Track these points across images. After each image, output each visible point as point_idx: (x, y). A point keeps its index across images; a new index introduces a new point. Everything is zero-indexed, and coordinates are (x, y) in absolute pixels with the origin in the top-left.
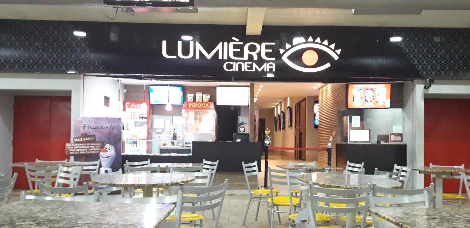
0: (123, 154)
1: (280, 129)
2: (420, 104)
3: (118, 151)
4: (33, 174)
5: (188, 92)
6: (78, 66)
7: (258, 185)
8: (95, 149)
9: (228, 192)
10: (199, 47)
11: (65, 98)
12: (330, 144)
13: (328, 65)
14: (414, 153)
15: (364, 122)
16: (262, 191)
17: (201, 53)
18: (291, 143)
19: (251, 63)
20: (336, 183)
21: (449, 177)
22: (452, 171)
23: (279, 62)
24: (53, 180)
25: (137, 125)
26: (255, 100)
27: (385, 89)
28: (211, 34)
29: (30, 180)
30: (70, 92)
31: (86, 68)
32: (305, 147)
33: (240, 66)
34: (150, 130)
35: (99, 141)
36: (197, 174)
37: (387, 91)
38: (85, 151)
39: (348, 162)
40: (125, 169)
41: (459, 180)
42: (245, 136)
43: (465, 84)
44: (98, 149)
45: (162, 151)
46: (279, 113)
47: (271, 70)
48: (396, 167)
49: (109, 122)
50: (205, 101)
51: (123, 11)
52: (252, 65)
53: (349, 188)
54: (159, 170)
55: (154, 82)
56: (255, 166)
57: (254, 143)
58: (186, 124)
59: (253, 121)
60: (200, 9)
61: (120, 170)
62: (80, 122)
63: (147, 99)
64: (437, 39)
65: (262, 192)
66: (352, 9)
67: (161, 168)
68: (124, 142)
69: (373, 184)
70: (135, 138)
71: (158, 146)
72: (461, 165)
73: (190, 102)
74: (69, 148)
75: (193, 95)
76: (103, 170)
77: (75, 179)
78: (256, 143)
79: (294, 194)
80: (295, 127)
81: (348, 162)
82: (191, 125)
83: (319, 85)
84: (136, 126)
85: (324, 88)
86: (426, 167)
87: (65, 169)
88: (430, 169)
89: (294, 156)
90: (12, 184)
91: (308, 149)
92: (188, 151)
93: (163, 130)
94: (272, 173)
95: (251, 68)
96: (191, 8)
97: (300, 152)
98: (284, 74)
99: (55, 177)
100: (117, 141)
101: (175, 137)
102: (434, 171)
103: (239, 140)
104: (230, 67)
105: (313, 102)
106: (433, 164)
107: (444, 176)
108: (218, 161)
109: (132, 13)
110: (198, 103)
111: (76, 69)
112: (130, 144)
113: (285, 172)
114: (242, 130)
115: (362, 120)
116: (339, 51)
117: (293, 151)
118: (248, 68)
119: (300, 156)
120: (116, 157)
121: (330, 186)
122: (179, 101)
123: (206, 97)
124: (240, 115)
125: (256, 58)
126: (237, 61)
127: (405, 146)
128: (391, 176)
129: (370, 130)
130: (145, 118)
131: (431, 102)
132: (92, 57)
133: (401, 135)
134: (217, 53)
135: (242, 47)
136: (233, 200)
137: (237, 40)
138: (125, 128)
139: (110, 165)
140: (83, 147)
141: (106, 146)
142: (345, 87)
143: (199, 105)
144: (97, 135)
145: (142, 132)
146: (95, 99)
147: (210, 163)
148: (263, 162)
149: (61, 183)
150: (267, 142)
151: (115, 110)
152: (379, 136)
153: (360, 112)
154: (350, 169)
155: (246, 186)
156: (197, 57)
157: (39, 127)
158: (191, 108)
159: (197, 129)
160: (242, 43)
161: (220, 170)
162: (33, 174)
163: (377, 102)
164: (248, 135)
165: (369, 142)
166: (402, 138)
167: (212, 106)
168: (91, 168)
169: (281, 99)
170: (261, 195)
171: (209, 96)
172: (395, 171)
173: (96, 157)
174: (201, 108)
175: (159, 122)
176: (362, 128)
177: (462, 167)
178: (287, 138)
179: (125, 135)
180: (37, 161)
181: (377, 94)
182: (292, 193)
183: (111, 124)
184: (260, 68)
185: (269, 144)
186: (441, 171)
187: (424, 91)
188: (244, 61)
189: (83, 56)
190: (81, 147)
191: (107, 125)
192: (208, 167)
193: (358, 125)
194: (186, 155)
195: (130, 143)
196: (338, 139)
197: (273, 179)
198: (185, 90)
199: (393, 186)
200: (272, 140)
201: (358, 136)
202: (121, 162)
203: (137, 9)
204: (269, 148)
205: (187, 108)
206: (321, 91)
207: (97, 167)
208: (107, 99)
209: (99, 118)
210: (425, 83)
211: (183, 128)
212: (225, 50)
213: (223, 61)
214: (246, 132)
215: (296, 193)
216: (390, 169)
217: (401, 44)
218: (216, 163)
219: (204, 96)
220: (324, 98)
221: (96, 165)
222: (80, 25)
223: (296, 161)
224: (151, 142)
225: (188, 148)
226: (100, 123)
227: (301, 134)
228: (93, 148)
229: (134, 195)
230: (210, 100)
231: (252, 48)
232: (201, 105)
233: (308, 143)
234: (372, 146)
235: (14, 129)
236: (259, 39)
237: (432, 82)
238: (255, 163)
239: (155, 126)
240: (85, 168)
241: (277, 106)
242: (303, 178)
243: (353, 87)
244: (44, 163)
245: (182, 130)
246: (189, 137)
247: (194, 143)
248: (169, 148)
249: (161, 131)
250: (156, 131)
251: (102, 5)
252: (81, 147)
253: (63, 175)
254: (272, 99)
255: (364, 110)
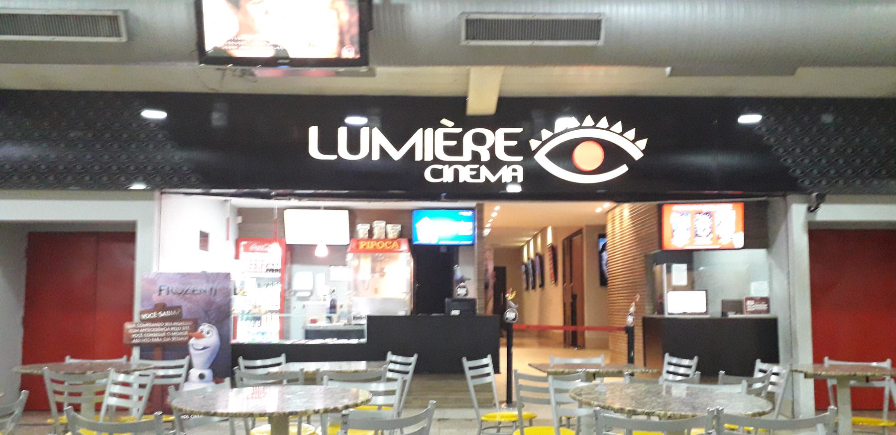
0: (233, 341)
1: (534, 288)
2: (800, 240)
3: (224, 337)
4: (59, 388)
5: (358, 220)
6: (150, 175)
7: (493, 398)
8: (181, 333)
9: (437, 414)
10: (380, 139)
11: (124, 236)
12: (630, 319)
13: (623, 169)
14: (792, 334)
15: (695, 273)
16: (504, 414)
17: (383, 151)
18: (556, 317)
19: (476, 166)
20: (644, 405)
21: (863, 384)
22: (869, 374)
23: (529, 163)
24: (97, 399)
25: (262, 284)
26: (486, 232)
27: (734, 212)
28: (402, 115)
29: (53, 399)
30: (133, 224)
31: (168, 179)
32: (583, 324)
33: (456, 172)
34: (287, 294)
35: (189, 317)
36: (374, 386)
37: (737, 215)
38: (162, 338)
39: (667, 355)
40: (237, 376)
41: (882, 389)
42: (468, 304)
43: (886, 203)
44: (186, 333)
45: (309, 334)
46: (532, 255)
47: (515, 179)
48: (759, 365)
49: (208, 281)
50: (391, 236)
51: (234, 76)
52: (478, 170)
53: (670, 417)
54: (301, 378)
55: (294, 202)
56: (486, 366)
57: (484, 318)
58: (355, 280)
59: (481, 272)
60: (380, 70)
61: (227, 380)
62: (152, 282)
63: (278, 236)
64: (827, 119)
65: (502, 417)
66: (665, 66)
67: (307, 373)
68: (235, 319)
69: (717, 410)
70: (256, 311)
71: (301, 325)
72: (883, 360)
73: (362, 240)
74: (131, 331)
75: (367, 226)
76: (195, 373)
77: (140, 398)
78: (490, 317)
79: (564, 422)
80: (564, 282)
81: (667, 355)
82: (364, 282)
83: (607, 205)
84: (259, 285)
85: (617, 210)
86: (818, 365)
87: (122, 378)
88: (827, 370)
89: (562, 339)
90: (17, 412)
91: (589, 329)
92: (358, 334)
93: (312, 293)
94: (521, 382)
95: (477, 176)
96: (363, 69)
97: (574, 334)
98: (540, 186)
99: (102, 393)
100: (220, 314)
101: (333, 308)
102: (833, 373)
103: (456, 312)
104: (437, 174)
105: (596, 236)
106: (831, 358)
107: (852, 382)
108: (416, 356)
109: (250, 78)
110: (378, 240)
111: (145, 180)
112: (248, 321)
113: (545, 380)
114: (461, 292)
115: (690, 269)
116: (643, 143)
117: (561, 331)
118: (472, 177)
119: (573, 339)
120: (220, 348)
121: (634, 413)
122: (344, 238)
123: (393, 230)
124: (457, 263)
125: (485, 157)
126: (451, 164)
127: (774, 322)
128: (750, 386)
129: (707, 291)
130: (277, 270)
131: (818, 235)
132: (176, 158)
133: (766, 300)
134: (412, 150)
135: (459, 138)
136: (446, 431)
137: (452, 124)
138: (238, 291)
139: (208, 365)
140: (158, 330)
141: (201, 328)
142: (656, 210)
143: (380, 245)
144: (186, 306)
145: (271, 297)
146: (182, 237)
147: (400, 359)
148: (503, 351)
149: (112, 406)
150: (510, 315)
151: (220, 257)
152: (724, 303)
153: (687, 256)
154: (672, 368)
155: (470, 401)
156: (376, 156)
157: (74, 291)
158: (366, 251)
159: (376, 291)
160: (459, 130)
161: (419, 370)
162: (59, 388)
163: (718, 238)
164: (472, 302)
165: (706, 313)
166: (768, 306)
167: (405, 247)
168: (171, 372)
169: (535, 230)
170: (500, 423)
171: (398, 227)
172: (758, 375)
173: (178, 350)
174: (384, 251)
175: (303, 277)
176: (692, 286)
177: (887, 364)
178: (548, 305)
179: (238, 306)
180: (69, 360)
181: (716, 224)
182: (561, 418)
183: (210, 286)
184: (494, 174)
185: (514, 320)
186: (847, 373)
187: (806, 218)
188: (464, 164)
189: (159, 157)
190: (154, 330)
191: (204, 286)
192: (397, 367)
193: (684, 282)
194: (354, 341)
195: (247, 319)
196: (647, 308)
197: (523, 393)
198: (354, 217)
199: (756, 410)
200: (520, 311)
201: (683, 303)
202: (230, 362)
203: (260, 72)
204: (514, 327)
205: (357, 250)
206: (610, 215)
207: (182, 371)
208: (204, 237)
209: (188, 274)
210: (807, 201)
211: (349, 289)
212: (428, 143)
213: (424, 164)
214: (468, 297)
215: (569, 418)
216: (748, 372)
217: (760, 129)
218: (413, 360)
219: (389, 227)
220: (617, 230)
221: (182, 367)
222: (154, 100)
223: (566, 350)
224: (288, 318)
225: (358, 328)
226: (190, 284)
227: (574, 297)
228: (176, 332)
229: (253, 427)
230: (401, 235)
231: (479, 140)
232: (384, 245)
233: (589, 316)
234: (712, 321)
235: (28, 278)
236: (492, 122)
237: (821, 199)
238: (488, 360)
239: (295, 286)
240: (161, 372)
241: (528, 242)
242: (580, 395)
243: (671, 212)
244: (82, 365)
245: (349, 292)
246: (361, 308)
247: (370, 318)
248: (321, 328)
249: (308, 294)
250: (299, 294)
251: (197, 63)
252: (154, 330)
253: (117, 389)
254: (519, 231)
255: (695, 253)
